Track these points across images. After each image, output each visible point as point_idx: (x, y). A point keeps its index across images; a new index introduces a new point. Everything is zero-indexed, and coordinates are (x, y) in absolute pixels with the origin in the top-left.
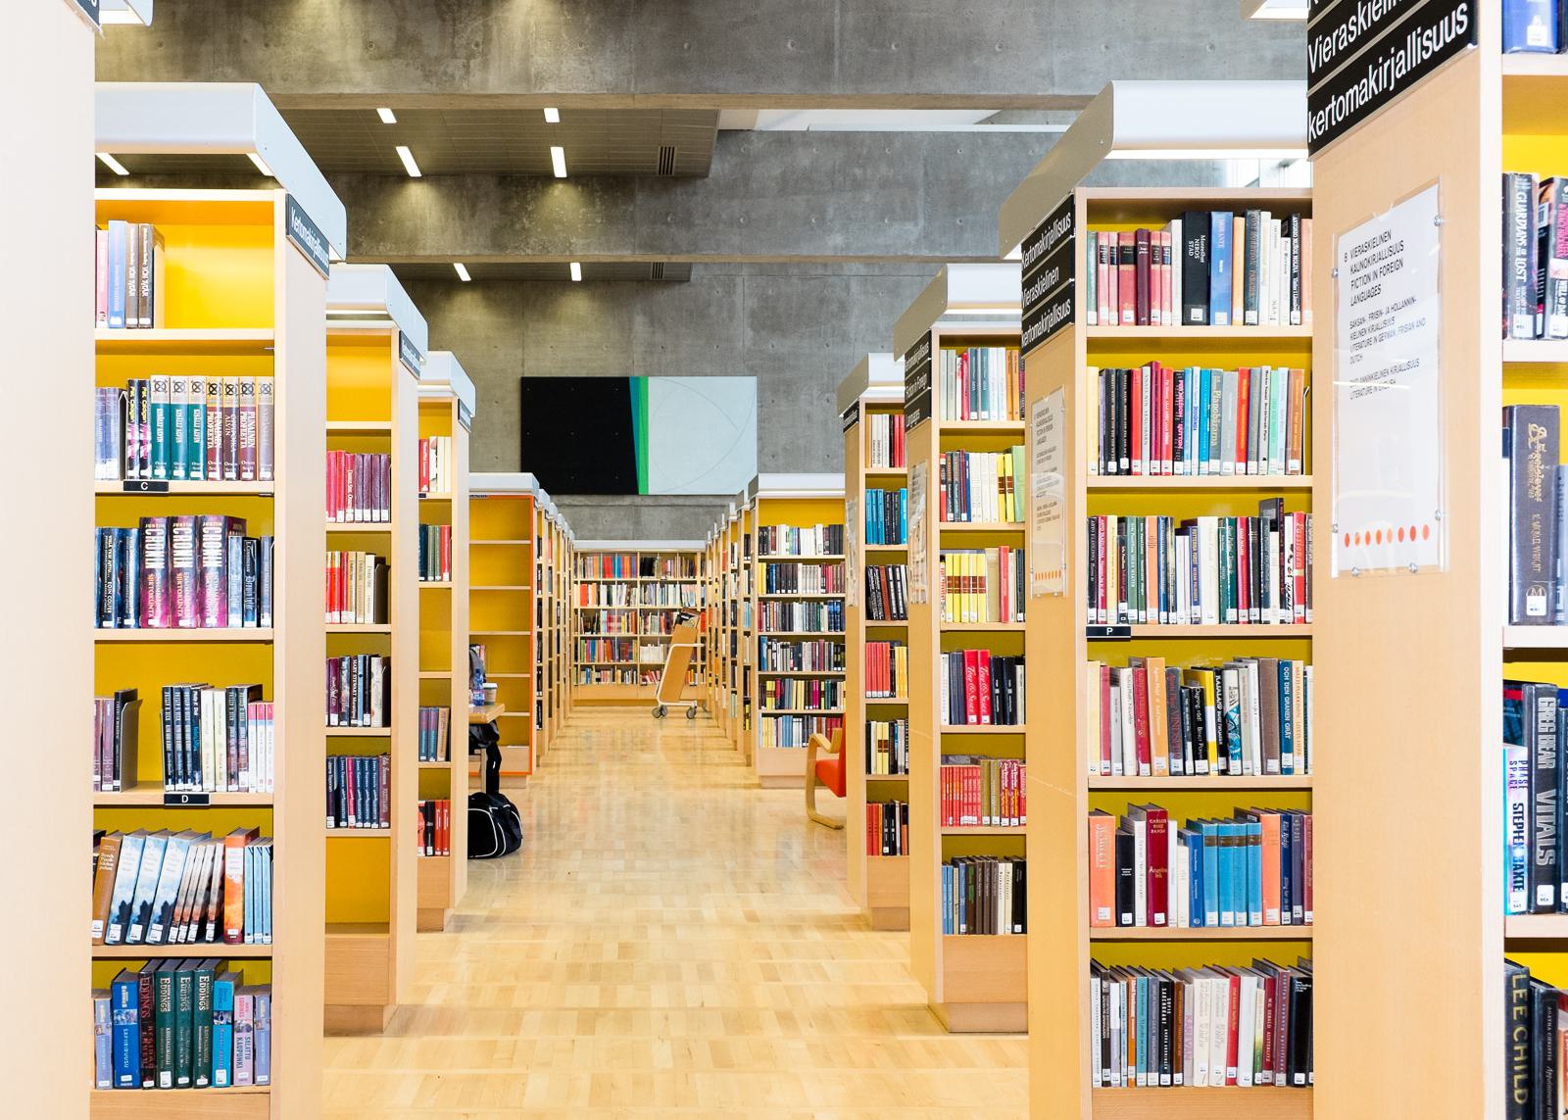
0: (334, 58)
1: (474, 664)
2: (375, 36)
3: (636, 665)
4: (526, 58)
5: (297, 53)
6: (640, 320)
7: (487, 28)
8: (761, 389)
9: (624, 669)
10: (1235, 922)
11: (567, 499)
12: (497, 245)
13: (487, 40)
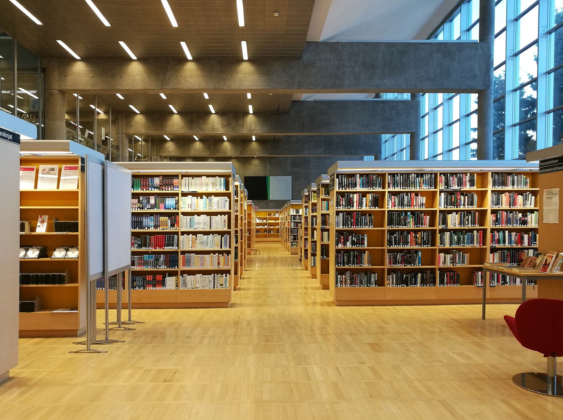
0: (216, 127)
1: (205, 230)
2: (224, 123)
3: (178, 232)
4: (250, 127)
5: (210, 126)
6: (268, 165)
7: (243, 122)
8: (292, 178)
9: (354, 272)
10: (221, 213)
11: (256, 201)
12: (242, 153)
13: (244, 124)
